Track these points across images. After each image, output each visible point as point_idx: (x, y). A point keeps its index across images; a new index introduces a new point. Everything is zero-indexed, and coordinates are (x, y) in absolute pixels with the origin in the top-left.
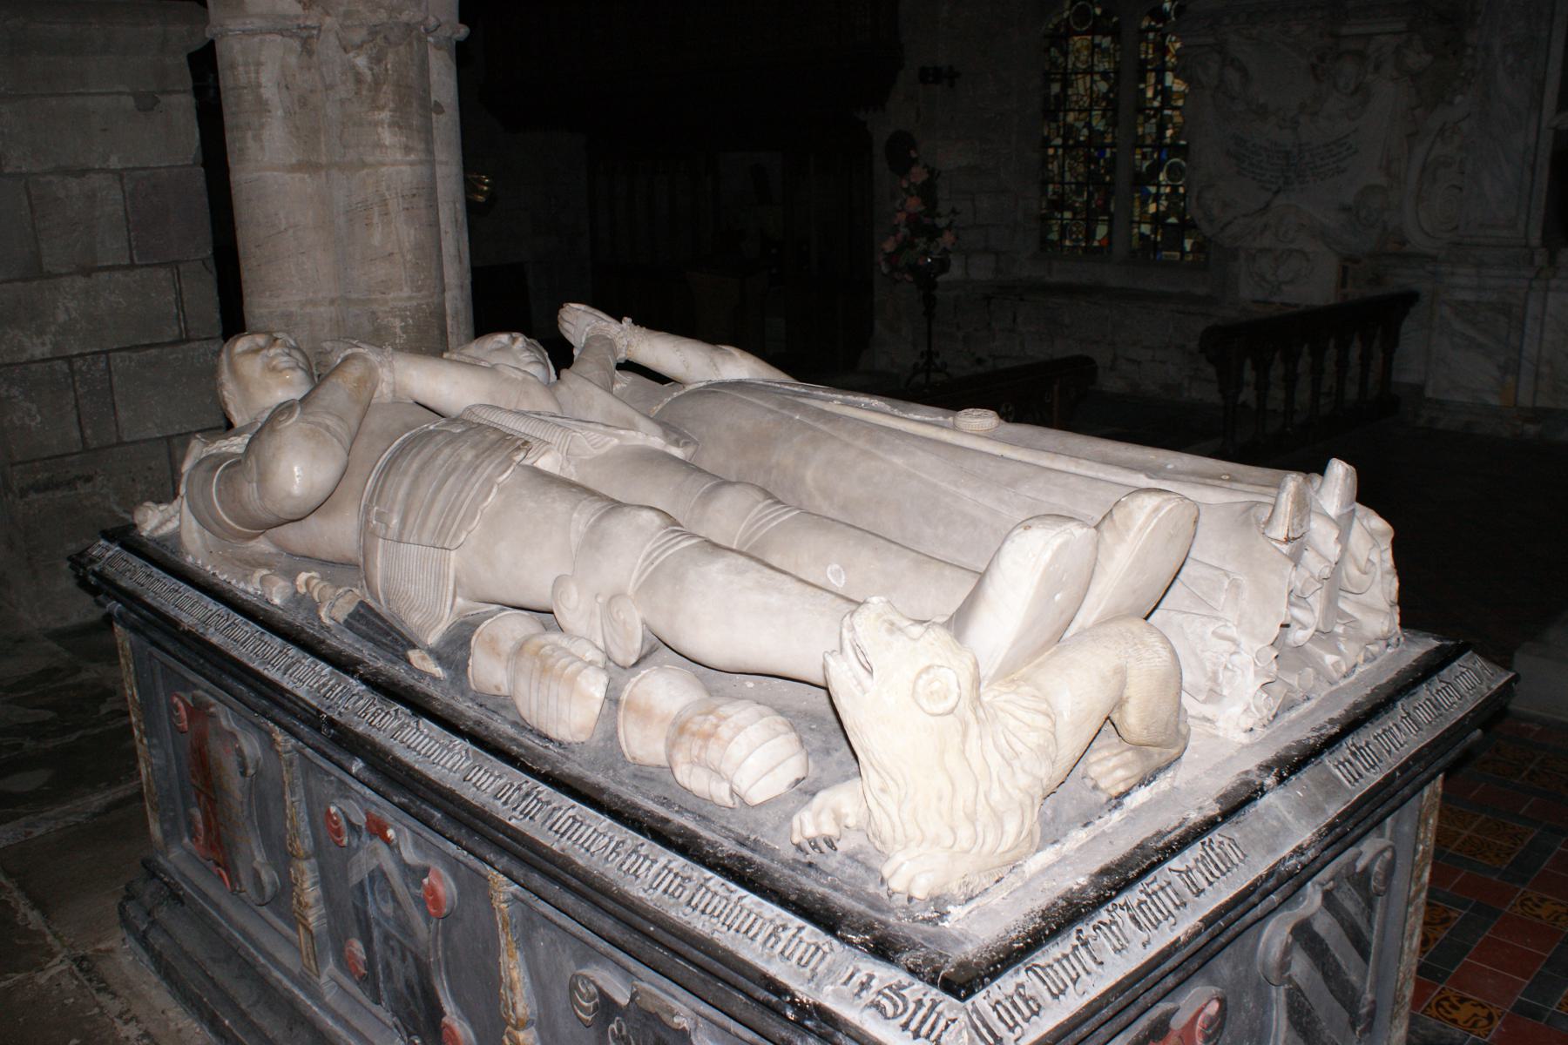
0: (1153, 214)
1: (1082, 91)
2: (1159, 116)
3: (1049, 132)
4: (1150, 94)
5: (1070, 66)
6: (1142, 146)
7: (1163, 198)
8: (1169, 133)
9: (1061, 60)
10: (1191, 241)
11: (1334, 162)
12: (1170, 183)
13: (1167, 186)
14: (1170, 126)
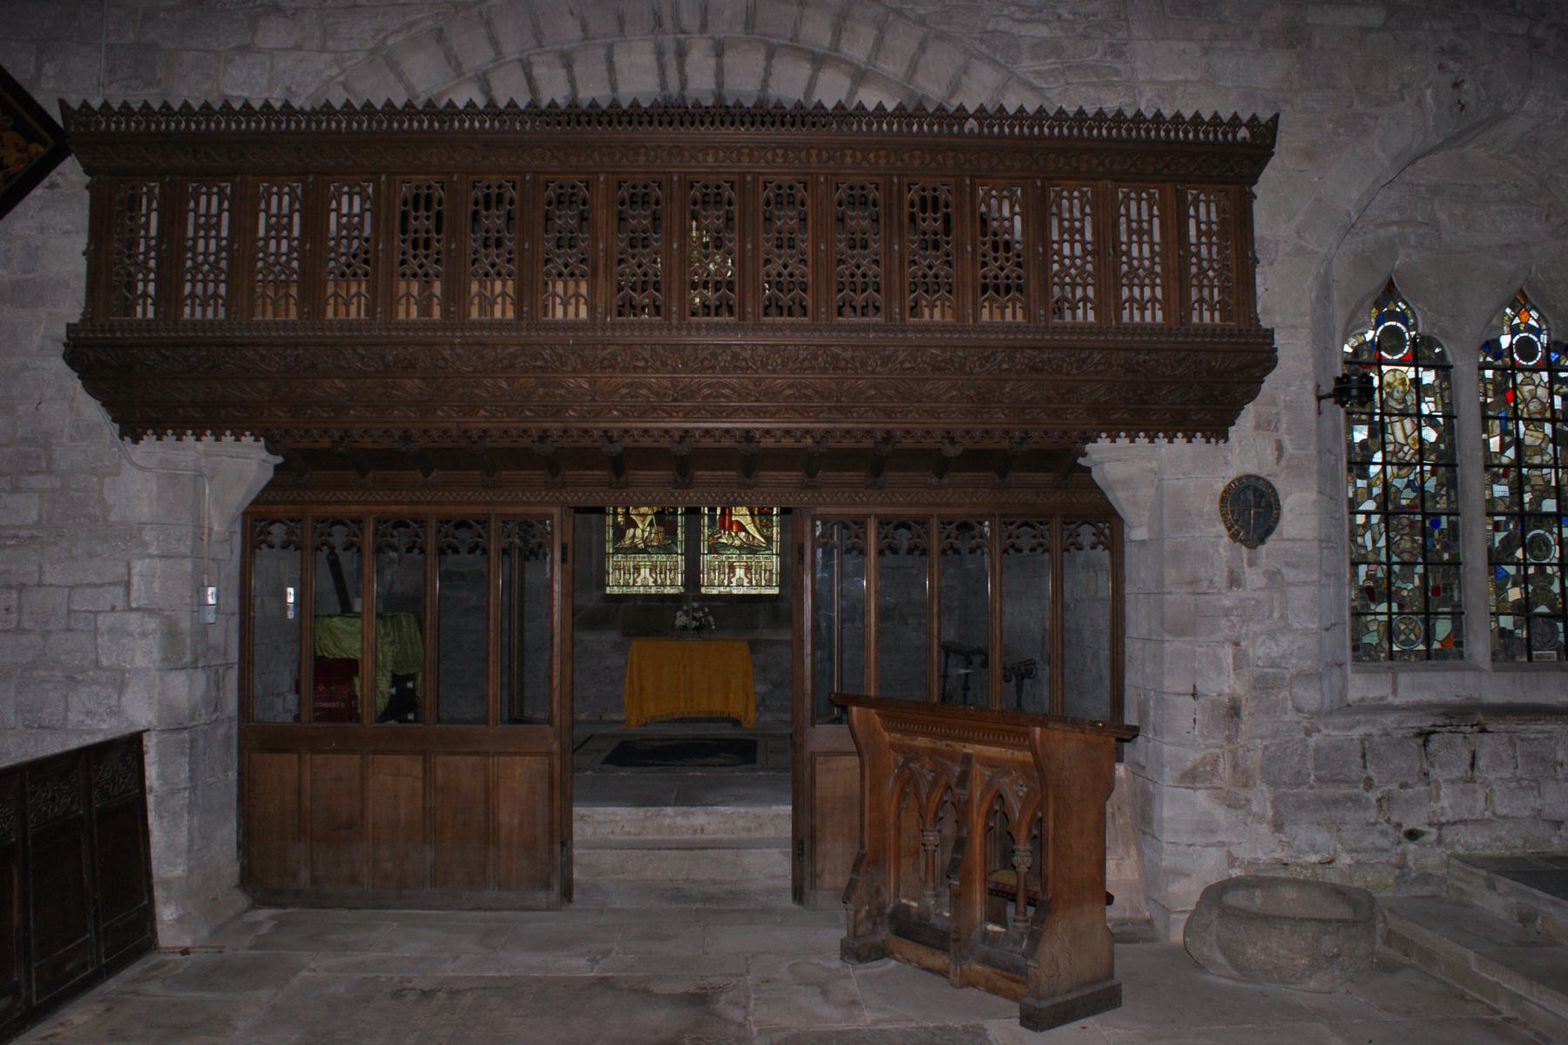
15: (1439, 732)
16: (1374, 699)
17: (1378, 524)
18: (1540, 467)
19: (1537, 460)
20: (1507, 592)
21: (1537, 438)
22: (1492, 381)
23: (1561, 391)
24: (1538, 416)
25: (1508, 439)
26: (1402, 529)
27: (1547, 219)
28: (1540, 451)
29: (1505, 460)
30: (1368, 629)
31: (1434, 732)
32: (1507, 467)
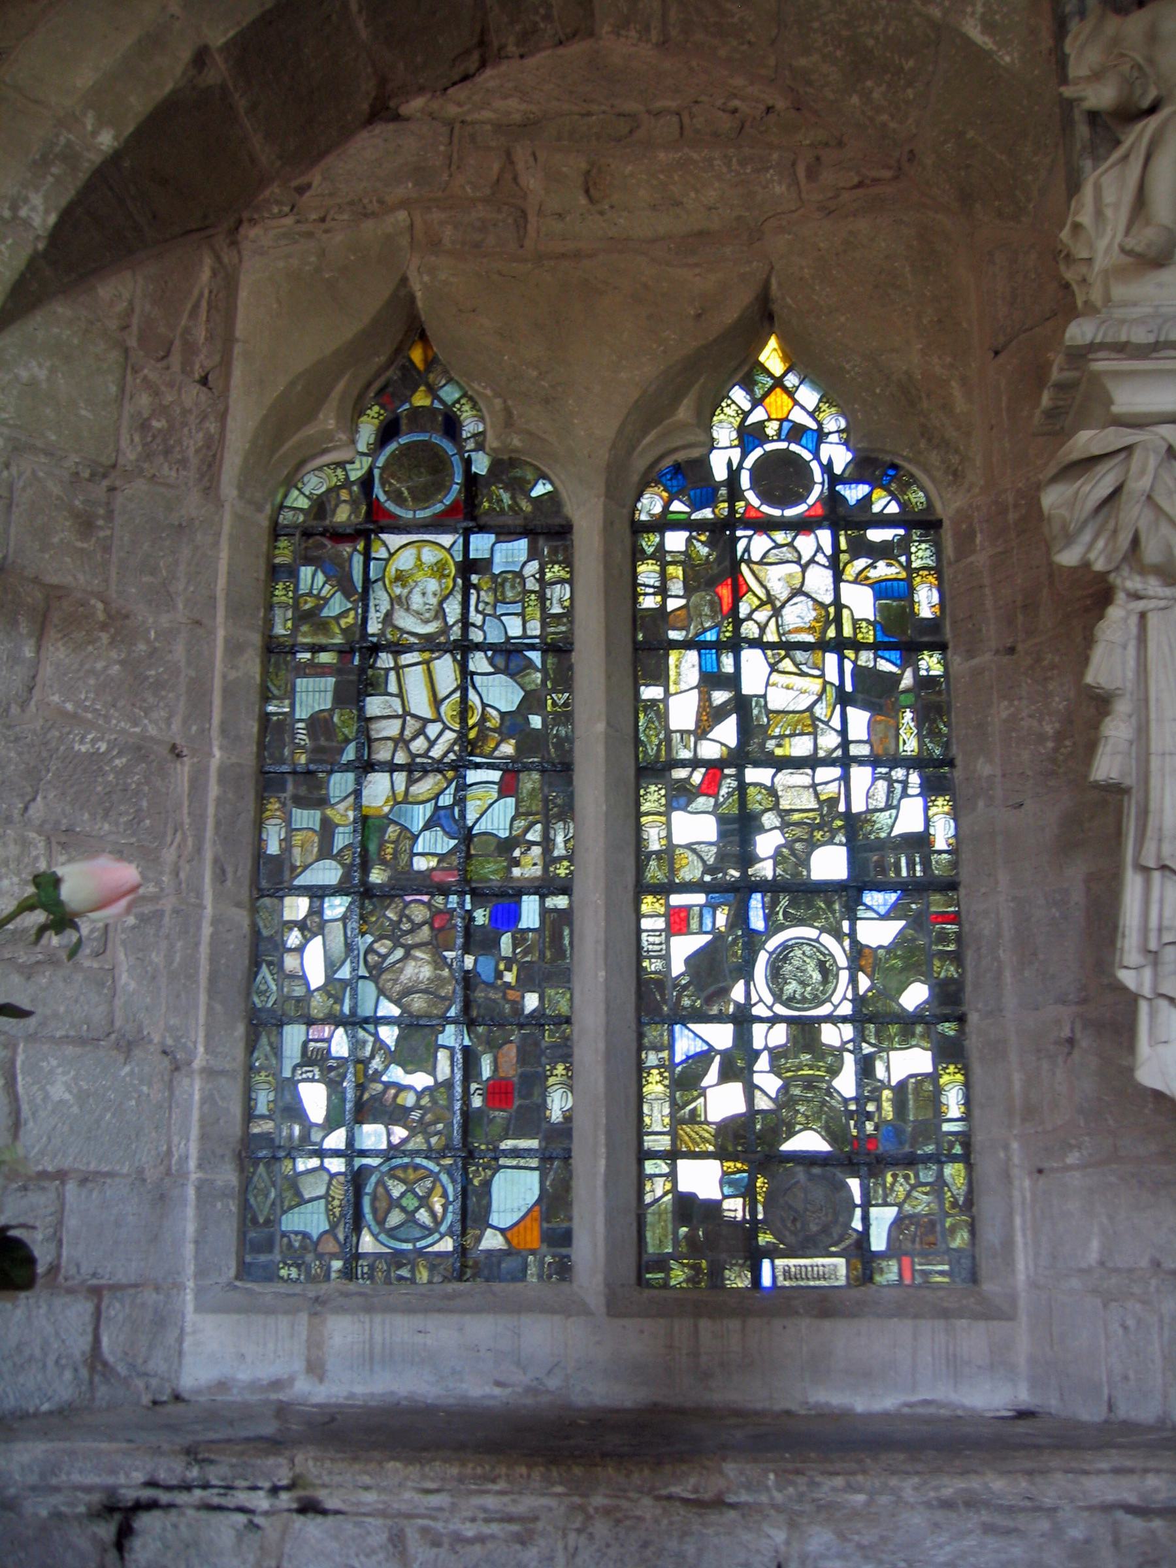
1: (420, 704)
3: (287, 844)
5: (373, 627)
6: (664, 890)
8: (767, 844)
9: (337, 605)
12: (781, 1010)
13: (774, 1020)
14: (770, 819)
15: (170, 1506)
16: (254, 1386)
17: (344, 919)
18: (811, 762)
19: (800, 747)
20: (703, 1094)
21: (803, 692)
22: (687, 559)
23: (873, 574)
24: (809, 638)
25: (720, 697)
26: (410, 932)
27: (812, 174)
28: (810, 723)
29: (709, 750)
30: (298, 1193)
31: (152, 1505)
32: (714, 767)
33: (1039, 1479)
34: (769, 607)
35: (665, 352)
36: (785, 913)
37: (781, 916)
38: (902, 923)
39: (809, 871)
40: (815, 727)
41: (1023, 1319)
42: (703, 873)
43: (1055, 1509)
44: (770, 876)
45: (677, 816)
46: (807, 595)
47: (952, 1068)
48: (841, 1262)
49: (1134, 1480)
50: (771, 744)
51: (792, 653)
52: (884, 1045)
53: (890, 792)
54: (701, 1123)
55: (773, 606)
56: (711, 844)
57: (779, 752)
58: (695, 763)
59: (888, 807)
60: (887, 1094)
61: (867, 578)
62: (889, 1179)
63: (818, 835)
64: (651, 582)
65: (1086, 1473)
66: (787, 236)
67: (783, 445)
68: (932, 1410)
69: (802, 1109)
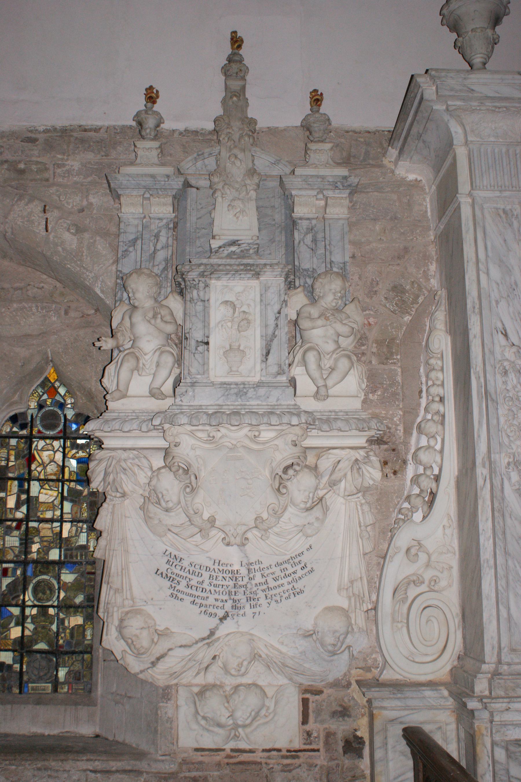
0: (15, 640)
2: (23, 527)
4: (11, 503)
7: (29, 620)
8: (35, 547)
10: (66, 670)
11: (289, 583)
13: (34, 606)
14: (36, 539)
18: (52, 521)
19: (49, 515)
21: (51, 496)
23: (77, 455)
24: (54, 477)
25: (24, 497)
27: (66, 313)
28: (52, 506)
29: (19, 515)
32: (20, 522)
33: (64, 762)
34: (42, 466)
35: (9, 379)
36: (40, 571)
37: (38, 572)
38: (76, 575)
39: (48, 557)
40: (54, 508)
41: (99, 706)
42: (14, 557)
43: (69, 771)
44: (35, 558)
45: (7, 538)
46: (55, 462)
47: (89, 623)
48: (50, 685)
49: (92, 763)
50: (39, 514)
51: (48, 482)
52: (68, 615)
53: (77, 530)
54: (8, 639)
55: (44, 465)
56: (17, 547)
57: (41, 516)
58: (13, 520)
59: (76, 536)
60: (68, 631)
61: (75, 457)
62: (67, 658)
63: (52, 545)
64: (4, 456)
65: (78, 760)
66: (55, 336)
67: (52, 408)
68: (69, 734)
69: (41, 635)
